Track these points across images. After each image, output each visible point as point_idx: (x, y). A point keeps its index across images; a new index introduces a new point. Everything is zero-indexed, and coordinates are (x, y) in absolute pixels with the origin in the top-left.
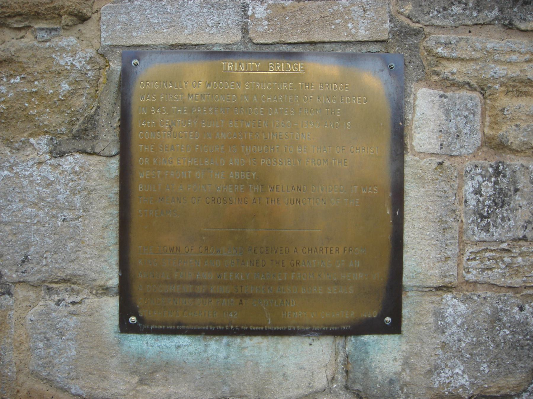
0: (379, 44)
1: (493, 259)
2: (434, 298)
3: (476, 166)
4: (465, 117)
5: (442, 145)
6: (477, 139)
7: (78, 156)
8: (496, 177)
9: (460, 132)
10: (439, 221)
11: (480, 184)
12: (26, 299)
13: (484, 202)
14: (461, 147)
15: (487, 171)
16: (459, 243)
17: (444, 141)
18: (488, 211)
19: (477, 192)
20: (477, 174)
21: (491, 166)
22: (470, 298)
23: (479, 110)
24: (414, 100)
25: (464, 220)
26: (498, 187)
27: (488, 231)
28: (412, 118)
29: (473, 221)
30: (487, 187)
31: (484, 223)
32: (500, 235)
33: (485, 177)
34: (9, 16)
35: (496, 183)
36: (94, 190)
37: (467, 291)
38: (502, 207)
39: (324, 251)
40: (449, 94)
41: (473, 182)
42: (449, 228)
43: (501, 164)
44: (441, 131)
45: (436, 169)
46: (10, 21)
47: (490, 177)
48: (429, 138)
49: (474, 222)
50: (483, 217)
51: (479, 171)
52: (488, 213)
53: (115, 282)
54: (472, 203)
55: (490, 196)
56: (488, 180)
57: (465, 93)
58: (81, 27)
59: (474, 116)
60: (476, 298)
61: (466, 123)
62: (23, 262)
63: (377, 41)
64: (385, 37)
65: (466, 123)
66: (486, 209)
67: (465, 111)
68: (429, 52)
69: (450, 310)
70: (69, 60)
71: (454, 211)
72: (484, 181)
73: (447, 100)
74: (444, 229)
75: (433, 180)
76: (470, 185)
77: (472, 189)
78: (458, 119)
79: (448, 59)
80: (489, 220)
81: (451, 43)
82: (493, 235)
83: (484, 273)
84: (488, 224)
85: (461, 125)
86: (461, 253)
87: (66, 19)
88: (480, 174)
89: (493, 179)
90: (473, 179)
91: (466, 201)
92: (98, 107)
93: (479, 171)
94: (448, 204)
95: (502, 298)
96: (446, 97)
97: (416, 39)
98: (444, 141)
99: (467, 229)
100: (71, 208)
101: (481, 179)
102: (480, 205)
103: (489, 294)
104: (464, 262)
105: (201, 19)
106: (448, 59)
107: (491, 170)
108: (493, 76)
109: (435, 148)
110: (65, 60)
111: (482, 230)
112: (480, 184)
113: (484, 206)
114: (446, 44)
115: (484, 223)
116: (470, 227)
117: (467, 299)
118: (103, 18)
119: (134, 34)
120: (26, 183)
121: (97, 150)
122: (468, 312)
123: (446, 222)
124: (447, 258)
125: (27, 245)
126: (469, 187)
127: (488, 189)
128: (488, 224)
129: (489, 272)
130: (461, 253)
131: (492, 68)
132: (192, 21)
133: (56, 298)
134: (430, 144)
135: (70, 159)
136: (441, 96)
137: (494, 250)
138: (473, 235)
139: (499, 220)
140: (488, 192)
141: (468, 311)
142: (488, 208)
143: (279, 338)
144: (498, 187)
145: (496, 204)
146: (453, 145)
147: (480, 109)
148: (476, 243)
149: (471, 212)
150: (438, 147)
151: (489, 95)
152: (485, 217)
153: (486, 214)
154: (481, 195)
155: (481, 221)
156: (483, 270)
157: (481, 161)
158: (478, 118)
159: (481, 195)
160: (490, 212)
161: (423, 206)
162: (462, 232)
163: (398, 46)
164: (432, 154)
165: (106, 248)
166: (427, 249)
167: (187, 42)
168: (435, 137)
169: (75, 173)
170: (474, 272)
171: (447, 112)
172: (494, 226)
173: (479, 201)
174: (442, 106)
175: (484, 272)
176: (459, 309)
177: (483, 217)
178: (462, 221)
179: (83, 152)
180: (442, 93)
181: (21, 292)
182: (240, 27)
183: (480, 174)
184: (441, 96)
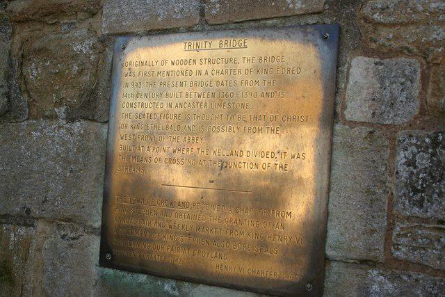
0: (316, 16)
1: (427, 238)
2: (358, 271)
3: (411, 136)
4: (402, 84)
5: (374, 113)
6: (414, 108)
7: (83, 122)
8: (433, 148)
9: (395, 99)
10: (366, 192)
11: (414, 155)
12: (43, 232)
13: (418, 174)
14: (396, 116)
15: (424, 141)
16: (388, 219)
17: (376, 109)
18: (422, 185)
19: (411, 163)
20: (411, 145)
21: (428, 136)
22: (399, 277)
23: (418, 77)
24: (349, 69)
25: (394, 192)
26: (435, 159)
27: (421, 206)
28: (346, 88)
29: (404, 194)
30: (423, 158)
31: (417, 197)
32: (436, 212)
33: (421, 147)
34: (46, 15)
35: (433, 155)
36: (92, 149)
37: (396, 269)
38: (440, 181)
39: (229, 72)
40: (386, 61)
41: (406, 153)
42: (377, 199)
43: (440, 134)
44: (374, 99)
45: (366, 138)
46: (47, 19)
47: (427, 148)
48: (361, 106)
49: (405, 196)
50: (416, 191)
51: (414, 141)
52: (422, 187)
53: (98, 224)
54: (404, 174)
55: (426, 168)
56: (423, 151)
57: (402, 60)
58: (91, 20)
59: (412, 82)
60: (406, 278)
61: (402, 90)
62: (44, 202)
63: (314, 13)
64: (320, 8)
65: (402, 90)
66: (420, 183)
67: (402, 78)
68: (366, 19)
69: (375, 287)
70: (79, 47)
71: (384, 183)
72: (419, 152)
73: (382, 67)
74: (371, 200)
75: (362, 149)
76: (403, 155)
77: (404, 160)
78: (394, 86)
79: (384, 25)
80: (423, 195)
81: (388, 8)
82: (427, 211)
83: (415, 253)
84: (422, 198)
85: (396, 93)
86: (390, 228)
87: (80, 15)
88: (416, 145)
89: (430, 150)
90: (406, 149)
91: (397, 173)
92: (98, 84)
93: (414, 141)
94: (376, 174)
95: (438, 282)
96: (382, 64)
97: (353, 7)
98: (376, 109)
99: (398, 201)
100: (76, 162)
101: (415, 150)
102: (414, 178)
103: (422, 276)
104: (393, 237)
105: (170, 7)
106: (384, 25)
107: (427, 140)
108: (436, 39)
109: (366, 117)
110: (77, 48)
111: (414, 204)
112: (414, 155)
113: (418, 178)
114: (383, 9)
115: (417, 197)
116: (401, 200)
117: (394, 278)
118: (104, 12)
119: (123, 24)
120: (50, 142)
121: (96, 118)
122: (396, 293)
123: (374, 193)
124: (373, 231)
125: (47, 189)
126: (401, 157)
127: (423, 161)
128: (422, 198)
129: (423, 252)
130: (390, 228)
131: (435, 30)
132: (164, 9)
133: (63, 233)
134: (362, 112)
135: (78, 124)
136: (376, 64)
137: (428, 228)
138: (404, 209)
139: (435, 196)
140: (423, 164)
141: (396, 291)
142: (423, 181)
143: (237, 291)
144: (435, 159)
145: (432, 177)
146: (386, 113)
147: (419, 75)
148: (408, 218)
149: (403, 184)
150: (370, 115)
151: (433, 60)
152: (419, 191)
153: (419, 187)
154: (415, 167)
155: (414, 194)
156: (414, 249)
157: (417, 131)
158: (417, 84)
159: (415, 167)
160: (424, 185)
161: (350, 176)
162: (391, 204)
163: (336, 16)
164: (363, 123)
165: (96, 196)
166: (353, 219)
167: (160, 27)
168: (367, 105)
169: (80, 135)
170: (404, 250)
171: (382, 80)
172: (429, 202)
173: (412, 173)
174: (376, 73)
175: (416, 250)
176: (386, 287)
177: (416, 191)
178: (392, 194)
179: (86, 118)
180: (378, 60)
181: (40, 225)
182: (198, 11)
183: (416, 145)
184: (376, 64)
